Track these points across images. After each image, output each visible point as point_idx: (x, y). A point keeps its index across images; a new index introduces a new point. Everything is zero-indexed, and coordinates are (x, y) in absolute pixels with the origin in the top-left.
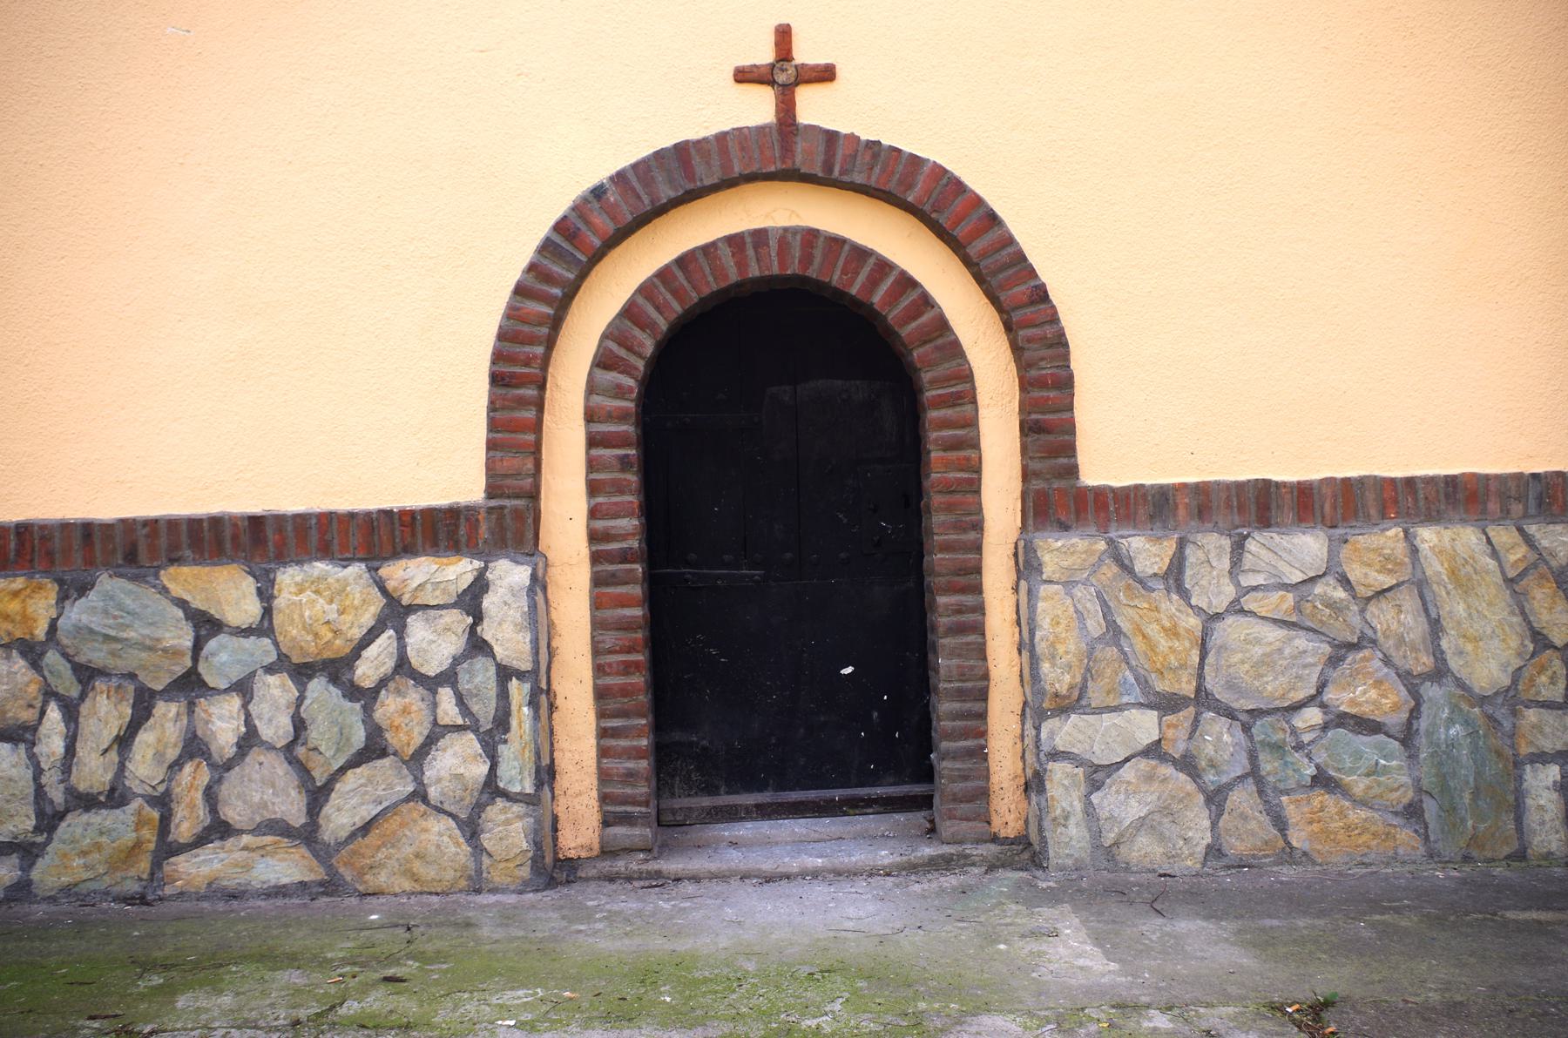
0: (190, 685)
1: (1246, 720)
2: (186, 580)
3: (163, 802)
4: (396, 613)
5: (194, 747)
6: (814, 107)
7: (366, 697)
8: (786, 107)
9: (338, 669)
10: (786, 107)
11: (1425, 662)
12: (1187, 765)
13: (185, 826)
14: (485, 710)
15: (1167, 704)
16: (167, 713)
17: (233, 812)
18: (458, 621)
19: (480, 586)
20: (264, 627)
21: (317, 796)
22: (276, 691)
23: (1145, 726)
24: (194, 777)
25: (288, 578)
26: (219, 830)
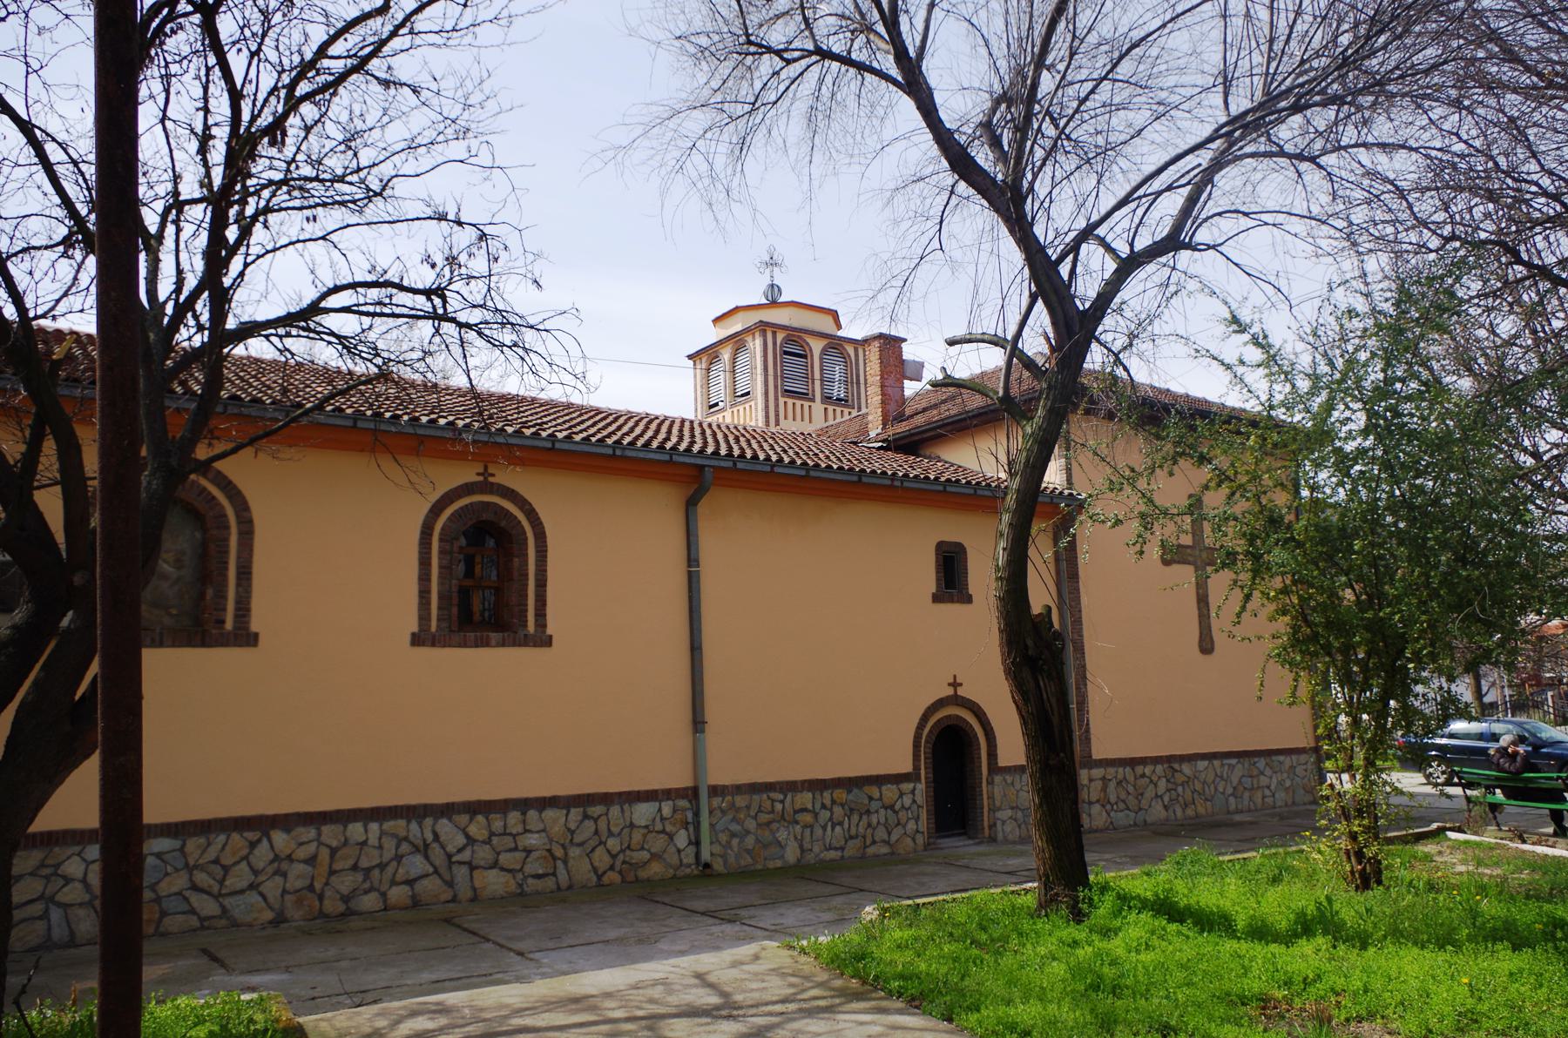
0: (868, 812)
1: (1023, 810)
2: (867, 789)
3: (864, 837)
4: (901, 795)
5: (869, 825)
6: (961, 692)
7: (896, 812)
8: (486, 468)
9: (892, 807)
10: (486, 468)
11: (227, 861)
12: (1015, 820)
13: (868, 843)
14: (915, 814)
15: (1012, 808)
16: (865, 817)
17: (876, 839)
18: (911, 796)
19: (914, 789)
20: (881, 799)
21: (889, 834)
22: (882, 811)
23: (1009, 813)
24: (869, 831)
25: (884, 788)
26: (874, 842)
